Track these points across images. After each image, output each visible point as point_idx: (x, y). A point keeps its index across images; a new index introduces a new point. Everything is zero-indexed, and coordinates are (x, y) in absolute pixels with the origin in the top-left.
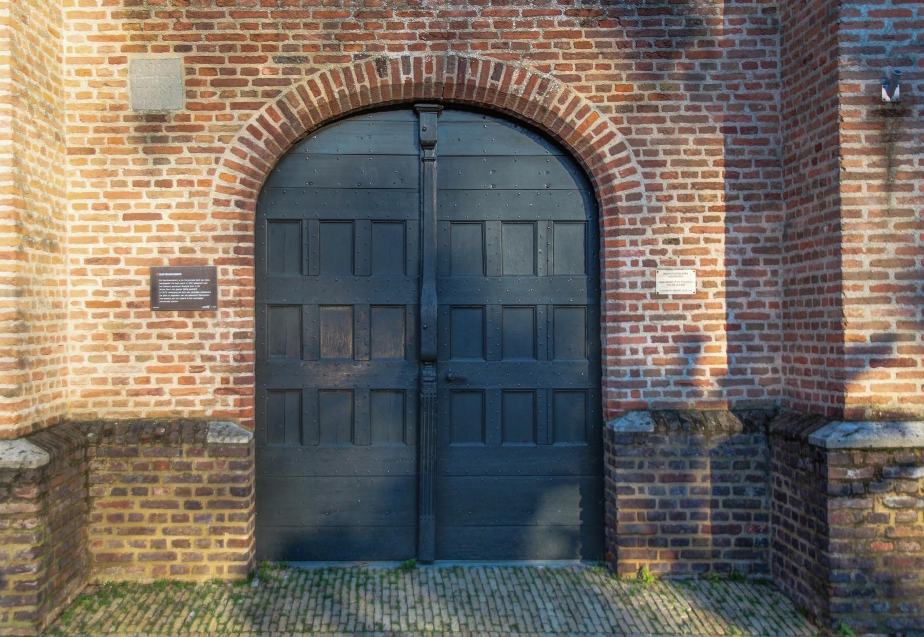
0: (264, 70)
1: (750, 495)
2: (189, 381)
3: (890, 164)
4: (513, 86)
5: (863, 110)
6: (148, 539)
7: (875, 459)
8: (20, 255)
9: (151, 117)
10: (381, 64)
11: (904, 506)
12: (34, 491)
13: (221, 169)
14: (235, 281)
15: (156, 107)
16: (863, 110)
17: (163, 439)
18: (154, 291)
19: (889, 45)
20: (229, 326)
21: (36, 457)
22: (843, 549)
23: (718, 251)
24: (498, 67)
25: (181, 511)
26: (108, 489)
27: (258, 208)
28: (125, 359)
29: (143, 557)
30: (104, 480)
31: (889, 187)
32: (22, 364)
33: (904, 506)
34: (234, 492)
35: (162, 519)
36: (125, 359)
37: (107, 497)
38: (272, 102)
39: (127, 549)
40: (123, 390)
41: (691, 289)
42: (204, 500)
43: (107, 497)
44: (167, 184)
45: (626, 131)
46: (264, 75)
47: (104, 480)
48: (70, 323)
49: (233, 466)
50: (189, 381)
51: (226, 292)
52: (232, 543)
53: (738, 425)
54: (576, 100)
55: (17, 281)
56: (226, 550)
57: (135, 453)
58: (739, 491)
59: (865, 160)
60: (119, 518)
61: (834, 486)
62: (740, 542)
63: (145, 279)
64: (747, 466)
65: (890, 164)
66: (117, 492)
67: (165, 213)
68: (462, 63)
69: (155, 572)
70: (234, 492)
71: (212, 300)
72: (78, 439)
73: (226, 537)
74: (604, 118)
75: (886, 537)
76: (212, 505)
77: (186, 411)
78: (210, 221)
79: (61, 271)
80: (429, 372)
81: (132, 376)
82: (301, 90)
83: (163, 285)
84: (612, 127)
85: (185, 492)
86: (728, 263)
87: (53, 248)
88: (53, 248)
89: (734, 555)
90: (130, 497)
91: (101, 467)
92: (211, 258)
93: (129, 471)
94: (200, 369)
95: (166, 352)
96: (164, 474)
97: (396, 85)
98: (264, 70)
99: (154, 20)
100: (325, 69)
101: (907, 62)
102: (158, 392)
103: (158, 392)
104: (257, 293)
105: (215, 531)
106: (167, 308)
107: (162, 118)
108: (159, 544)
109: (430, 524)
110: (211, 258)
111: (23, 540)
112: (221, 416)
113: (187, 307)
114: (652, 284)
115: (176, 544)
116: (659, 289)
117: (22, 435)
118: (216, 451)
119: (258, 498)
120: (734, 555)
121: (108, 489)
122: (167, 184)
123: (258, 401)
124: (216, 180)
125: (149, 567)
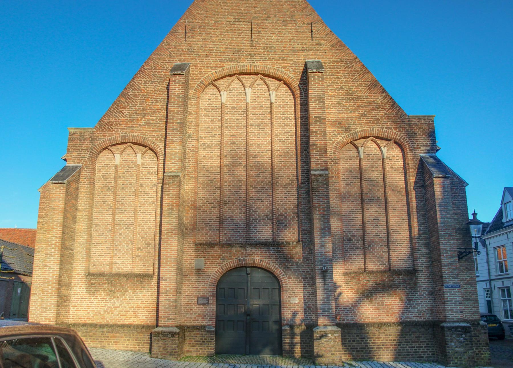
0: (218, 261)
1: (308, 341)
2: (203, 318)
3: (325, 280)
4: (264, 264)
5: (320, 271)
6: (195, 348)
7: (322, 333)
8: (176, 295)
9: (198, 270)
10: (240, 260)
11: (327, 341)
12: (178, 336)
13: (210, 279)
14: (213, 300)
15: (199, 268)
16: (320, 271)
17: (199, 329)
18: (198, 301)
19: (324, 260)
20: (212, 308)
21: (178, 330)
22: (316, 349)
23: (302, 295)
24: (261, 260)
25: (201, 343)
26: (188, 338)
27: (217, 286)
28: (192, 314)
29: (194, 351)
30: (188, 336)
31: (325, 285)
32: (435, 299)
33: (327, 341)
34: (211, 339)
35: (198, 344)
36: (192, 314)
37: (188, 340)
38: (220, 267)
39: (191, 350)
40: (191, 320)
41: (297, 302)
42: (205, 341)
43: (188, 340)
44: (201, 282)
45: (285, 272)
46: (218, 262)
47: (188, 336)
48: (182, 307)
49: (211, 334)
50: (203, 318)
51: (211, 302)
52: (210, 349)
53: (306, 328)
54: (275, 267)
55: (176, 300)
56: (209, 350)
57: (193, 331)
58: (306, 341)
59: (320, 280)
60: (190, 344)
61: (315, 338)
62: (306, 351)
63: (196, 299)
64: (307, 336)
65: (325, 280)
66: (190, 339)
67: (200, 287)
68: (254, 260)
69: (196, 354)
70: (211, 339)
71: (208, 303)
72: (183, 329)
73: (209, 348)
74: (280, 270)
75: (324, 347)
76: (207, 342)
77: (203, 324)
78: (208, 288)
79: (182, 298)
80: (248, 317)
81: (193, 317)
82: (225, 265)
83: (199, 300)
84: (282, 271)
85: (202, 339)
86: (304, 297)
87: (181, 293)
88: (181, 293)
89: (305, 353)
90: (192, 340)
91: (187, 334)
92: (208, 295)
93: (192, 335)
94: (205, 316)
95: (408, 348)
96: (198, 336)
97: (242, 264)
98: (218, 261)
99: (199, 252)
100: (229, 261)
101: (327, 263)
102: (198, 320)
103: (198, 320)
104: (216, 302)
105: (207, 347)
106: (200, 305)
107: (200, 270)
108: (197, 349)
109: (248, 348)
110: (208, 295)
111: (176, 344)
112: (209, 325)
113: (203, 304)
114: (289, 301)
115: (200, 349)
116: (291, 302)
117: (177, 327)
118: (208, 331)
119: (216, 341)
120: (305, 353)
121: (188, 338)
122: (201, 282)
123: (216, 322)
124: (209, 281)
125: (195, 353)
